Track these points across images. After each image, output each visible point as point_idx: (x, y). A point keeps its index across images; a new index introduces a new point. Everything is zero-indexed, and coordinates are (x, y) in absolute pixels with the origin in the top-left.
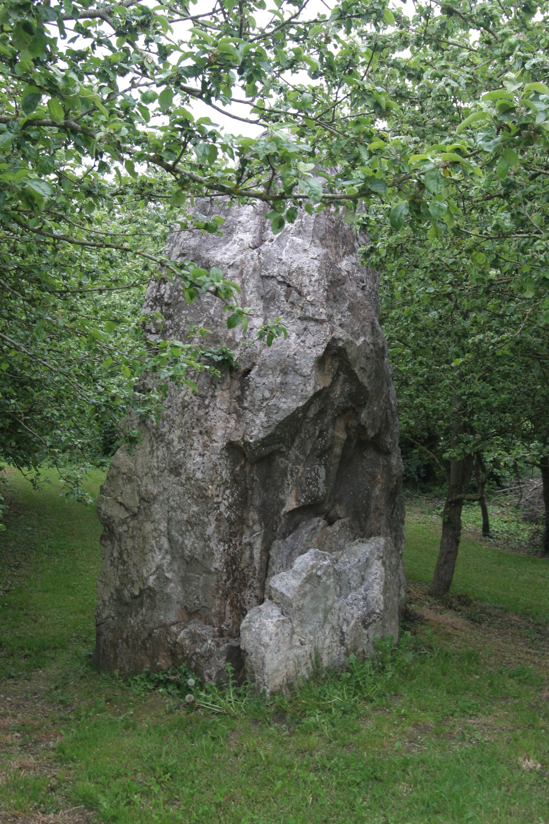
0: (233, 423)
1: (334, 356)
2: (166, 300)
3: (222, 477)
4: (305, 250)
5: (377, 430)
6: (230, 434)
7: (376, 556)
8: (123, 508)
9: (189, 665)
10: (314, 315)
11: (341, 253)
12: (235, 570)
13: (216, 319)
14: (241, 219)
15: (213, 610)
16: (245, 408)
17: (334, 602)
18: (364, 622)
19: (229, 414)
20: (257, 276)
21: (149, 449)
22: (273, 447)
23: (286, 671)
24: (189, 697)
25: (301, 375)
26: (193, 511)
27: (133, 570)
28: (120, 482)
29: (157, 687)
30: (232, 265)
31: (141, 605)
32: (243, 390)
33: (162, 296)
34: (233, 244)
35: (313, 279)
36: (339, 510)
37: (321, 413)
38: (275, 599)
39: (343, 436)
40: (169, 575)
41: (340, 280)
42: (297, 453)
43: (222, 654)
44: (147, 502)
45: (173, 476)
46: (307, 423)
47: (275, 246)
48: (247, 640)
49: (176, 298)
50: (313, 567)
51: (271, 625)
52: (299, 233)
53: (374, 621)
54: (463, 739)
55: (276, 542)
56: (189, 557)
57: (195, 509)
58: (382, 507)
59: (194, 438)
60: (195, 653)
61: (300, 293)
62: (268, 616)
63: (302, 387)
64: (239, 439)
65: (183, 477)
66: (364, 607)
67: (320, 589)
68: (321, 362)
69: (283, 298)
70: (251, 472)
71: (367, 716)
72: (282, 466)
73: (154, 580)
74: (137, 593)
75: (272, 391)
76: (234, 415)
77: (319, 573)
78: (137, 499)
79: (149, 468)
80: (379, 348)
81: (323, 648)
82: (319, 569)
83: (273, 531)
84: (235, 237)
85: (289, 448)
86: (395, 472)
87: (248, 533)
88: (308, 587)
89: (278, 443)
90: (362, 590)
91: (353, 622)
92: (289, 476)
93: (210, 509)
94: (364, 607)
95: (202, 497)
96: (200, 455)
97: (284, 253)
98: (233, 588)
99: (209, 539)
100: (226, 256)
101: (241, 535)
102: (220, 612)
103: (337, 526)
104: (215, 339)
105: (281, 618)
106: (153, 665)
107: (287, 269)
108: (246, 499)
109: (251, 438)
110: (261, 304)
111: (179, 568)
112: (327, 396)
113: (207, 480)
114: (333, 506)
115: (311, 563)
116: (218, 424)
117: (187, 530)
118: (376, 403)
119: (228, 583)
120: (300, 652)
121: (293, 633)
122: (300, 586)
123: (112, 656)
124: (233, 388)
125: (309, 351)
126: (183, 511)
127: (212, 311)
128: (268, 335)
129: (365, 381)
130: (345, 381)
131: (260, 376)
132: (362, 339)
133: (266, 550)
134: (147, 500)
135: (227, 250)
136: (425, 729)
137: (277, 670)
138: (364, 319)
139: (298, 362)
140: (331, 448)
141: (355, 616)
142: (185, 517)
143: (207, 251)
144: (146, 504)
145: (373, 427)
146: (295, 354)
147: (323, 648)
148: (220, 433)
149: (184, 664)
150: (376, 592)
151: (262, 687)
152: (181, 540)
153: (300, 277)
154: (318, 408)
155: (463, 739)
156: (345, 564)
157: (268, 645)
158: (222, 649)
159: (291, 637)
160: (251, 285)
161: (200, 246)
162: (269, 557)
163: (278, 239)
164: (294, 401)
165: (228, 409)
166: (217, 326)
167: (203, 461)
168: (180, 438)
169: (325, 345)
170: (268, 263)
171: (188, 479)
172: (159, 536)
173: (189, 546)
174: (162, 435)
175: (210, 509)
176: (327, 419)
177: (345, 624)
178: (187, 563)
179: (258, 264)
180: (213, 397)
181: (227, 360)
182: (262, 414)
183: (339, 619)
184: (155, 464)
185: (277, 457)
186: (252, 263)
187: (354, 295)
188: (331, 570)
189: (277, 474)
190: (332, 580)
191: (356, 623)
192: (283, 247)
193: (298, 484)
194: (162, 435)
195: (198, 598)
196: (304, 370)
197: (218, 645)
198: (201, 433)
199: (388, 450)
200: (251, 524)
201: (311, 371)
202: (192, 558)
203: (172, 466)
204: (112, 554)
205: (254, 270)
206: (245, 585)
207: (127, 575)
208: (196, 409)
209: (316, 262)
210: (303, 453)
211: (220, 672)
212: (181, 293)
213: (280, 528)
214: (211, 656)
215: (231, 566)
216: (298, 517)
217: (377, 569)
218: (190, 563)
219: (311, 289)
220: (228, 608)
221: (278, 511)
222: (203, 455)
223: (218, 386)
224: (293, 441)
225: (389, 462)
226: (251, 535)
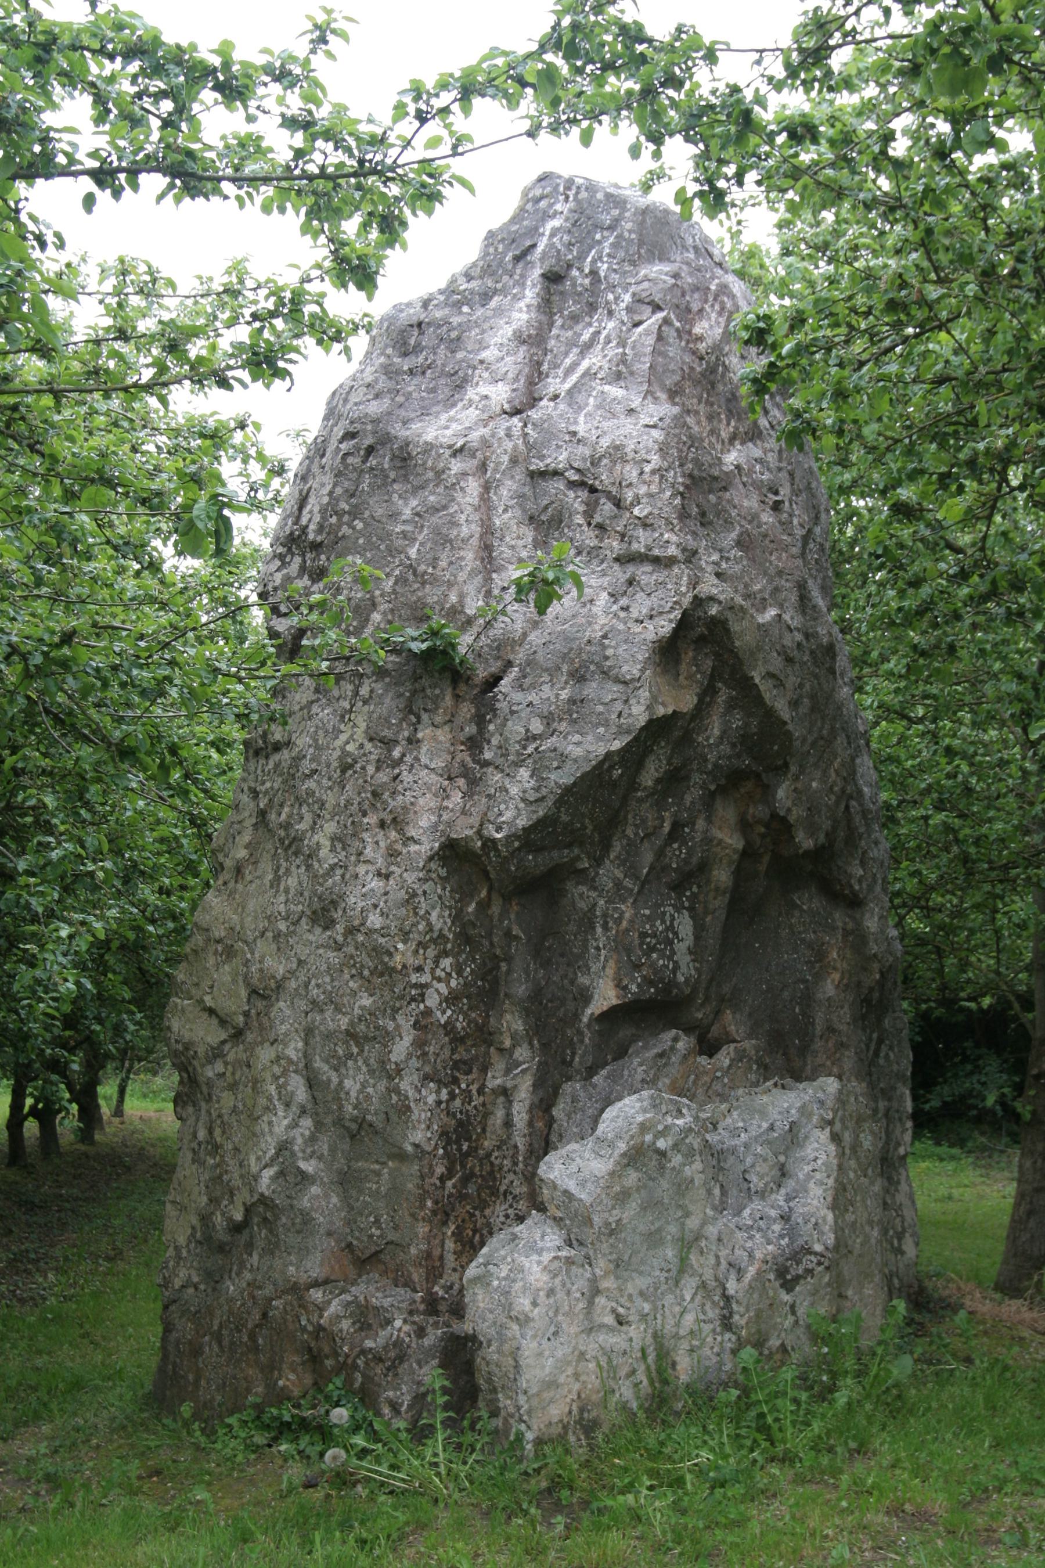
0: (456, 798)
1: (698, 640)
2: (311, 536)
3: (429, 924)
4: (631, 411)
5: (822, 838)
6: (450, 824)
7: (815, 1119)
8: (215, 1021)
9: (349, 1381)
10: (649, 549)
11: (724, 434)
12: (468, 1154)
13: (422, 568)
14: (484, 355)
15: (413, 1251)
16: (487, 764)
17: (703, 1224)
18: (781, 1273)
19: (450, 779)
20: (519, 474)
21: (270, 877)
22: (555, 854)
23: (577, 1386)
24: (334, 1455)
25: (617, 680)
26: (361, 1008)
27: (232, 1163)
28: (211, 961)
29: (275, 1439)
30: (461, 449)
31: (250, 1246)
32: (480, 721)
33: (304, 529)
34: (466, 408)
35: (648, 469)
36: (732, 1022)
37: (674, 780)
38: (552, 1210)
39: (734, 841)
40: (308, 1167)
41: (715, 479)
42: (619, 874)
43: (429, 1353)
44: (263, 997)
45: (318, 930)
46: (641, 800)
47: (562, 406)
48: (482, 1311)
49: (333, 531)
50: (644, 1128)
51: (536, 1268)
52: (618, 377)
53: (809, 1272)
54: (1023, 1544)
55: (567, 1087)
56: (354, 1120)
57: (366, 1001)
58: (843, 1028)
59: (365, 836)
60: (363, 1352)
61: (618, 503)
62: (533, 1249)
63: (619, 706)
64: (470, 832)
65: (340, 928)
66: (782, 1236)
67: (665, 1184)
68: (667, 653)
69: (579, 519)
70: (504, 914)
71: (771, 1494)
72: (582, 905)
73: (274, 1179)
74: (238, 1216)
75: (548, 719)
76: (461, 782)
77: (661, 1144)
78: (244, 993)
79: (269, 918)
80: (820, 646)
81: (676, 1336)
82: (662, 1134)
83: (564, 1062)
84: (471, 393)
85: (598, 862)
86: (874, 948)
87: (499, 1065)
88: (632, 1177)
89: (569, 845)
90: (780, 1198)
91: (752, 1271)
92: (599, 930)
93: (402, 997)
94: (782, 1236)
95: (382, 972)
96: (379, 874)
97: (581, 419)
98: (462, 1197)
99: (399, 1071)
100: (448, 432)
101: (484, 1069)
102: (429, 1255)
103: (724, 1058)
104: (419, 614)
105: (564, 1253)
106: (271, 1386)
107: (587, 452)
108: (496, 982)
109: (499, 829)
110: (529, 534)
111: (333, 1150)
112: (687, 739)
113: (393, 930)
114: (718, 1013)
115: (640, 1118)
116: (421, 801)
117: (350, 1056)
118: (818, 774)
119: (449, 1184)
120: (615, 1341)
121: (596, 1292)
122: (612, 1174)
123: (191, 1377)
124: (459, 721)
125: (637, 629)
126: (338, 1009)
127: (413, 552)
128: (541, 591)
129: (782, 707)
130: (731, 705)
131: (521, 688)
132: (772, 612)
133: (544, 1105)
134: (263, 993)
135: (451, 420)
136: (919, 1518)
137: (551, 1384)
138: (780, 573)
139: (609, 652)
140: (704, 867)
141: (759, 1255)
142: (344, 1022)
143: (404, 423)
144: (260, 1004)
145: (812, 829)
146: (605, 636)
147: (676, 1336)
148: (425, 821)
149: (338, 1382)
150: (814, 1201)
151: (515, 1427)
152: (335, 1080)
153: (618, 467)
154: (664, 767)
155: (1023, 1544)
156: (735, 1133)
157: (528, 1319)
158: (427, 1342)
159: (591, 1303)
160: (506, 491)
161: (389, 414)
162: (551, 1122)
163: (570, 392)
164: (600, 738)
165: (448, 768)
166: (423, 583)
167: (384, 886)
168: (334, 839)
169: (677, 614)
170: (545, 443)
171: (351, 931)
172: (285, 1073)
173: (353, 1094)
174: (297, 839)
175: (402, 997)
176: (692, 796)
177: (733, 1276)
178: (353, 1137)
179: (522, 447)
180: (413, 741)
181: (444, 652)
182: (524, 773)
183: (718, 1263)
184: (282, 908)
185: (569, 885)
186: (509, 445)
187: (754, 518)
188: (695, 1142)
189: (572, 927)
190: (698, 1165)
191: (759, 1273)
192: (580, 409)
193: (621, 946)
194: (297, 839)
195: (377, 1221)
196: (625, 669)
197: (421, 1332)
198: (382, 824)
199: (855, 894)
200: (508, 1043)
201: (643, 671)
202: (361, 1122)
203: (316, 905)
204: (195, 1135)
205: (514, 461)
206: (494, 1192)
207: (220, 1177)
208: (371, 769)
209: (656, 434)
210: (632, 872)
211: (420, 1399)
212: (346, 518)
213: (577, 1055)
214: (401, 1358)
215: (458, 1142)
216: (625, 1032)
217: (818, 1150)
218: (359, 1135)
219: (643, 490)
220: (450, 1245)
221: (577, 1016)
222: (387, 877)
223: (425, 717)
224: (607, 847)
225: (858, 924)
226: (508, 1071)
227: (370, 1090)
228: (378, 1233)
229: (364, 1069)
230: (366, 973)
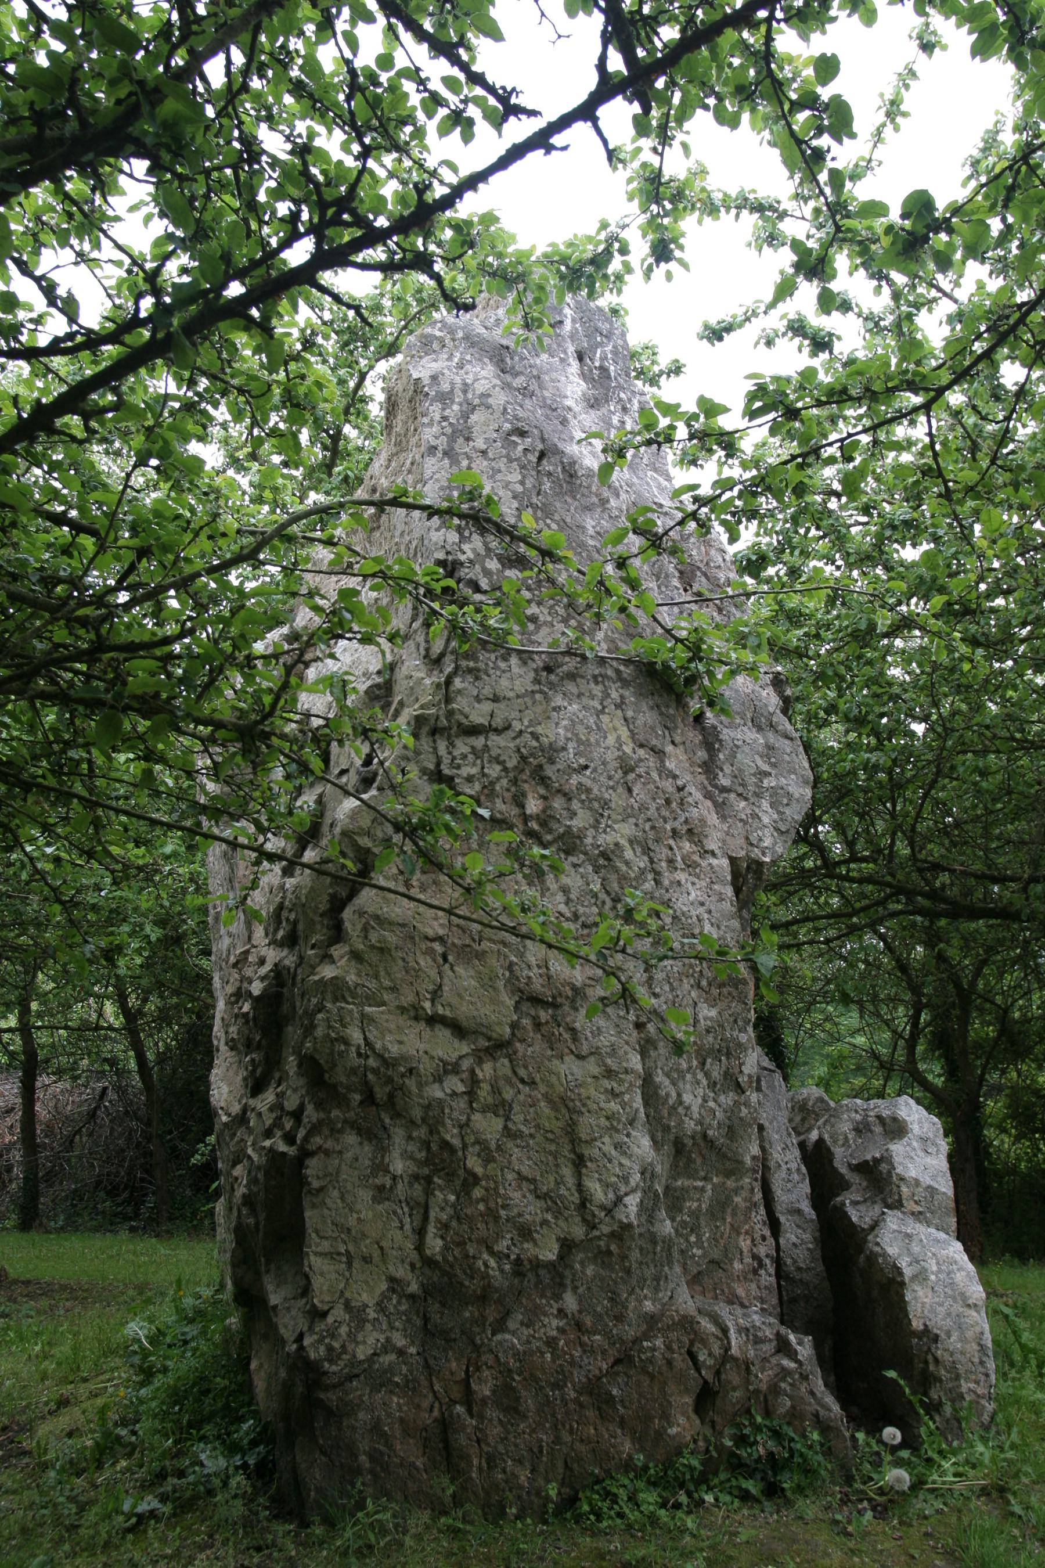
173: (695, 1109)
227: (712, 1104)
228: (699, 1252)
229: (705, 1082)
230: (704, 983)
